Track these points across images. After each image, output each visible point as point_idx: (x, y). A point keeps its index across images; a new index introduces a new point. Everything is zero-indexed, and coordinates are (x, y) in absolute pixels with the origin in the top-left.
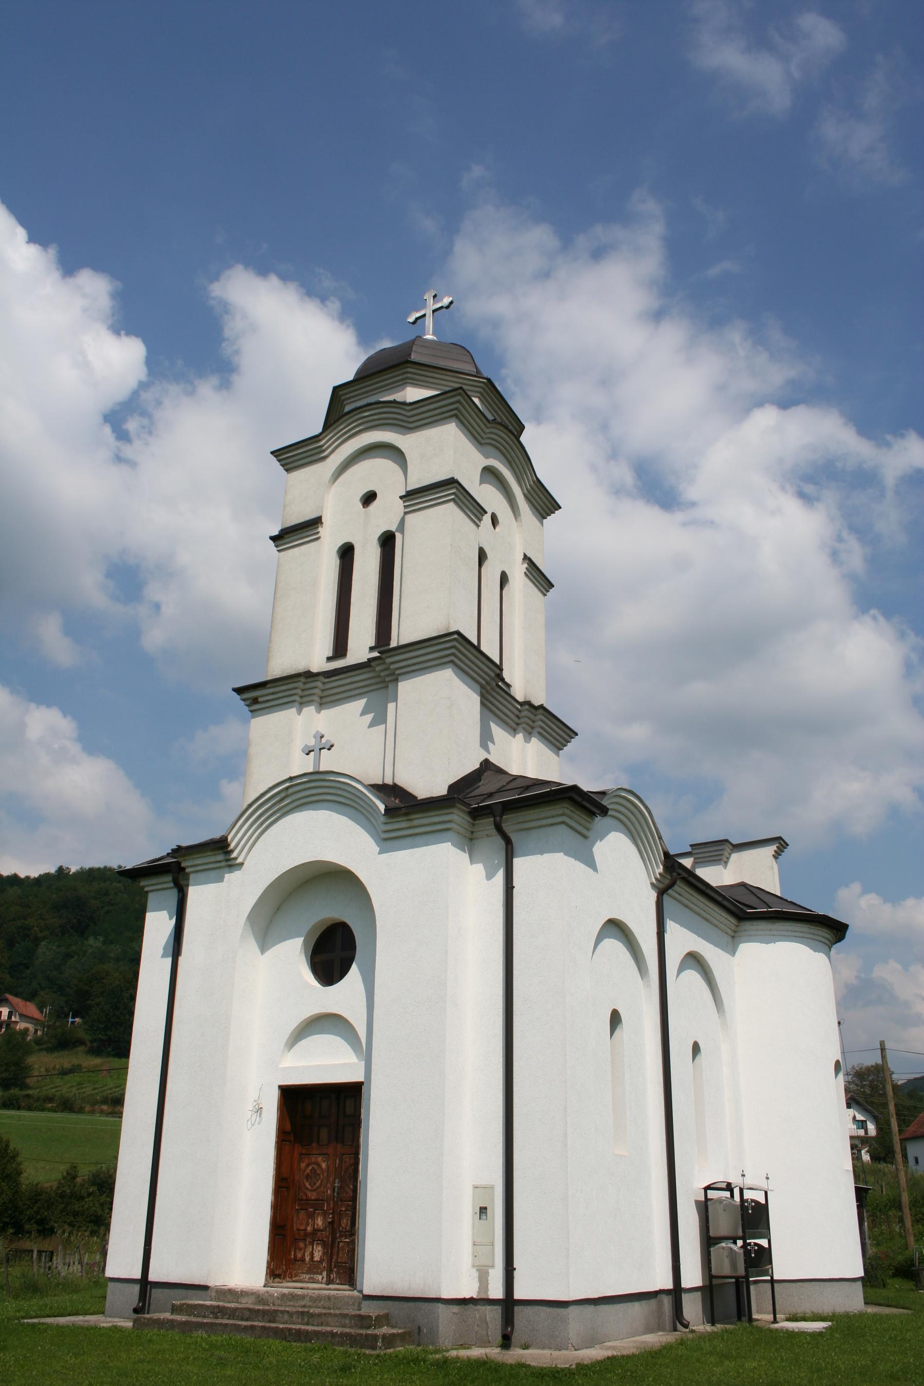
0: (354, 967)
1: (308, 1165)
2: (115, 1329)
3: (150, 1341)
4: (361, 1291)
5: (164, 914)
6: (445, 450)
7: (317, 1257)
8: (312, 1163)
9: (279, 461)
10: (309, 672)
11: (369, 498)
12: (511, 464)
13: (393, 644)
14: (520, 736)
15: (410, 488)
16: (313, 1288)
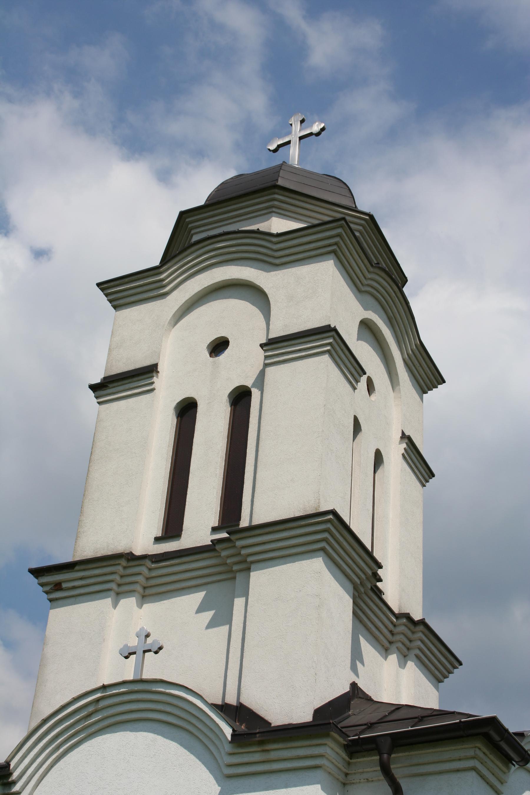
6: (317, 292)
9: (106, 295)
10: (131, 554)
11: (219, 346)
12: (391, 322)
13: (244, 523)
14: (393, 658)
15: (271, 336)
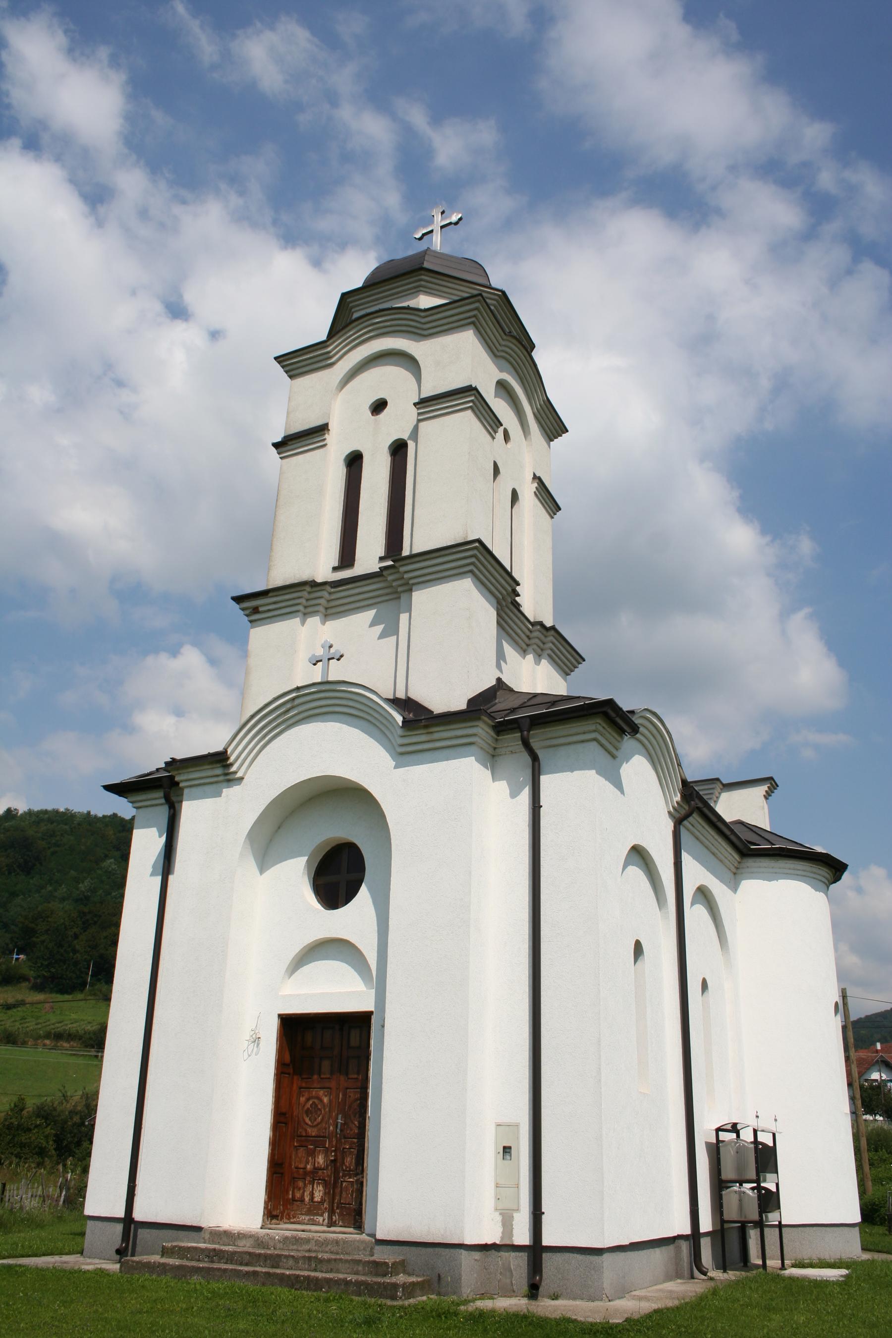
0: (364, 890)
1: (308, 1100)
2: (101, 1272)
3: (143, 1287)
4: (373, 1235)
5: (154, 831)
6: (459, 357)
7: (317, 1198)
8: (312, 1098)
9: (283, 367)
11: (379, 406)
13: (406, 552)
14: (530, 657)
15: (423, 396)
16: (315, 1230)
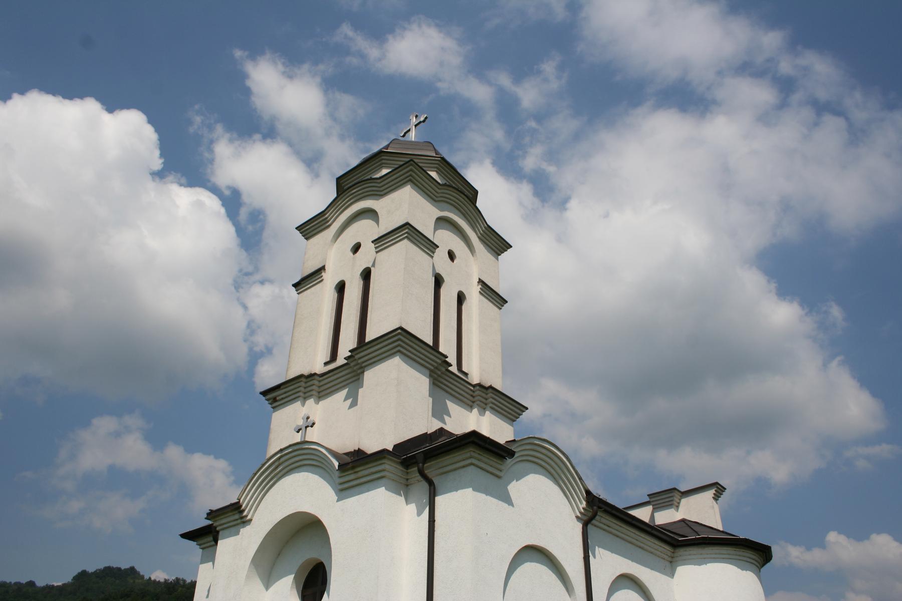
6: (405, 205)
11: (356, 248)
